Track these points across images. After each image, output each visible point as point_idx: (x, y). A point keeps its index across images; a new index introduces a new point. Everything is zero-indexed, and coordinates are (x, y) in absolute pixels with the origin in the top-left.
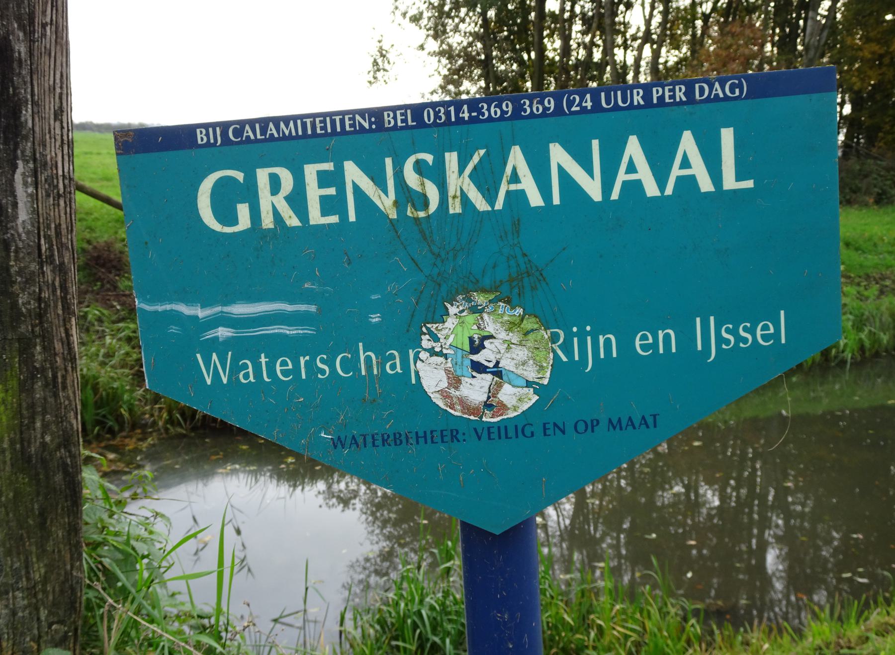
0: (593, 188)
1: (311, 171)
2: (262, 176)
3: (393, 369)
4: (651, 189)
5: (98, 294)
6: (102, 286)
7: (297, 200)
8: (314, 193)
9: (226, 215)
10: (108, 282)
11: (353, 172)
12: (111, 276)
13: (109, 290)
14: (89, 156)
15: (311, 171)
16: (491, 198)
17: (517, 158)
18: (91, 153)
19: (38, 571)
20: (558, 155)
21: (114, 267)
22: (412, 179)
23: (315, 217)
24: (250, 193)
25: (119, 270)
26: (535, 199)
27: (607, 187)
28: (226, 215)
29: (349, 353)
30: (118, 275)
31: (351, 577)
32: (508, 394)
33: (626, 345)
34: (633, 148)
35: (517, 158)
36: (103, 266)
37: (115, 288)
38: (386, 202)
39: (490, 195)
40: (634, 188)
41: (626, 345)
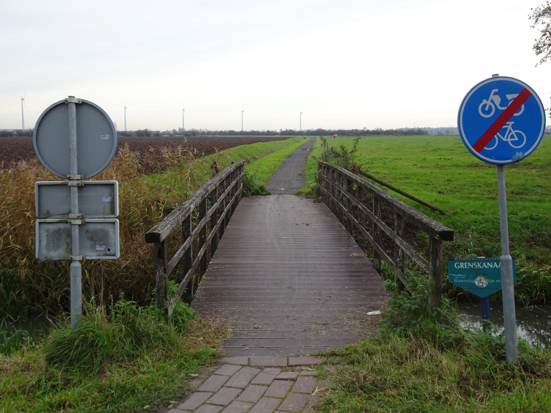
0: (492, 267)
1: (465, 263)
2: (461, 263)
3: (473, 282)
4: (497, 267)
5: (408, 239)
6: (410, 235)
7: (464, 266)
8: (466, 265)
9: (457, 267)
10: (412, 234)
11: (469, 264)
12: (413, 231)
13: (412, 237)
14: (396, 161)
15: (465, 263)
16: (482, 267)
17: (484, 264)
18: (397, 159)
19: (437, 300)
20: (488, 264)
21: (415, 227)
22: (475, 265)
23: (466, 267)
24: (460, 265)
25: (416, 229)
26: (486, 267)
27: (493, 267)
28: (457, 267)
29: (47, 319)
30: (416, 231)
31: (505, 350)
32: (484, 285)
33: (495, 281)
34: (495, 263)
35: (484, 264)
36: (410, 227)
37: (415, 236)
38: (472, 266)
39: (482, 267)
40: (495, 267)
41: (495, 281)
